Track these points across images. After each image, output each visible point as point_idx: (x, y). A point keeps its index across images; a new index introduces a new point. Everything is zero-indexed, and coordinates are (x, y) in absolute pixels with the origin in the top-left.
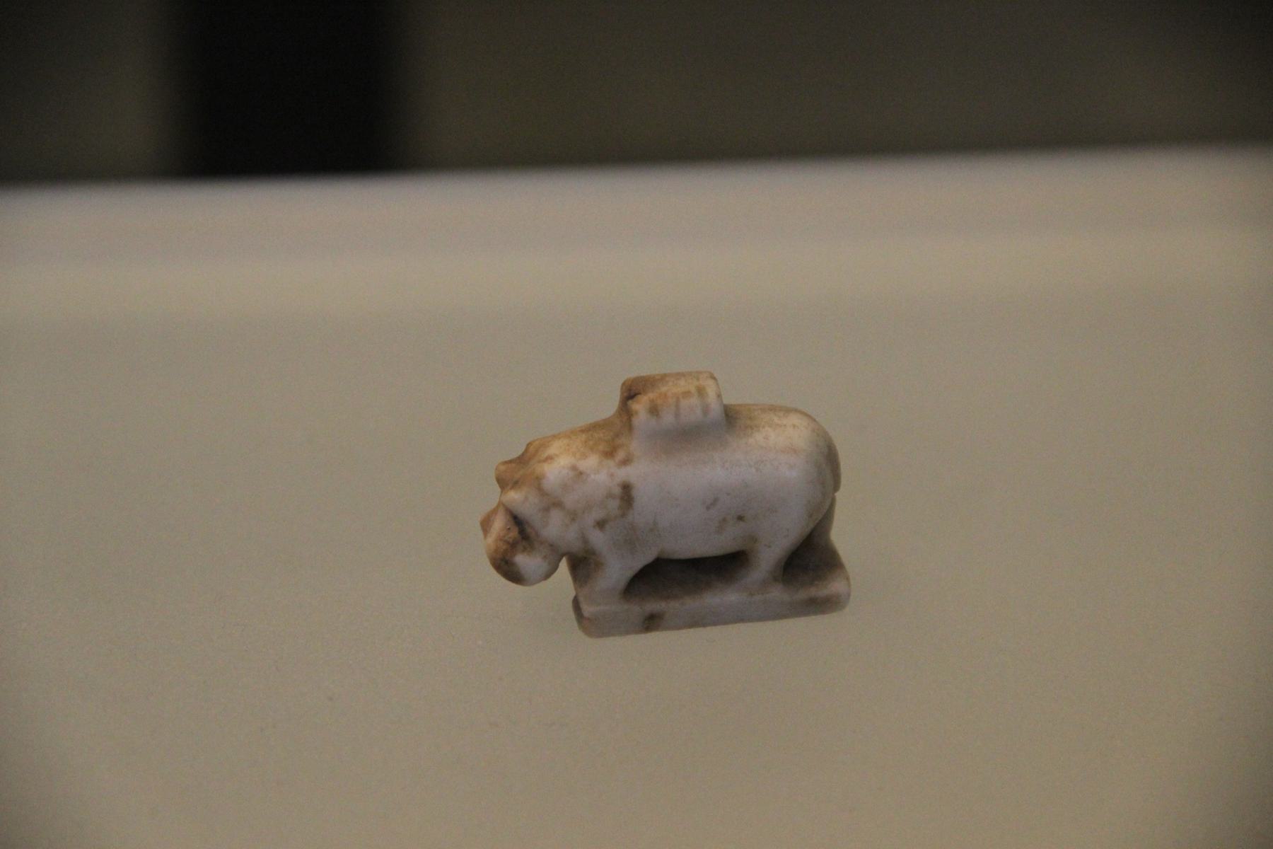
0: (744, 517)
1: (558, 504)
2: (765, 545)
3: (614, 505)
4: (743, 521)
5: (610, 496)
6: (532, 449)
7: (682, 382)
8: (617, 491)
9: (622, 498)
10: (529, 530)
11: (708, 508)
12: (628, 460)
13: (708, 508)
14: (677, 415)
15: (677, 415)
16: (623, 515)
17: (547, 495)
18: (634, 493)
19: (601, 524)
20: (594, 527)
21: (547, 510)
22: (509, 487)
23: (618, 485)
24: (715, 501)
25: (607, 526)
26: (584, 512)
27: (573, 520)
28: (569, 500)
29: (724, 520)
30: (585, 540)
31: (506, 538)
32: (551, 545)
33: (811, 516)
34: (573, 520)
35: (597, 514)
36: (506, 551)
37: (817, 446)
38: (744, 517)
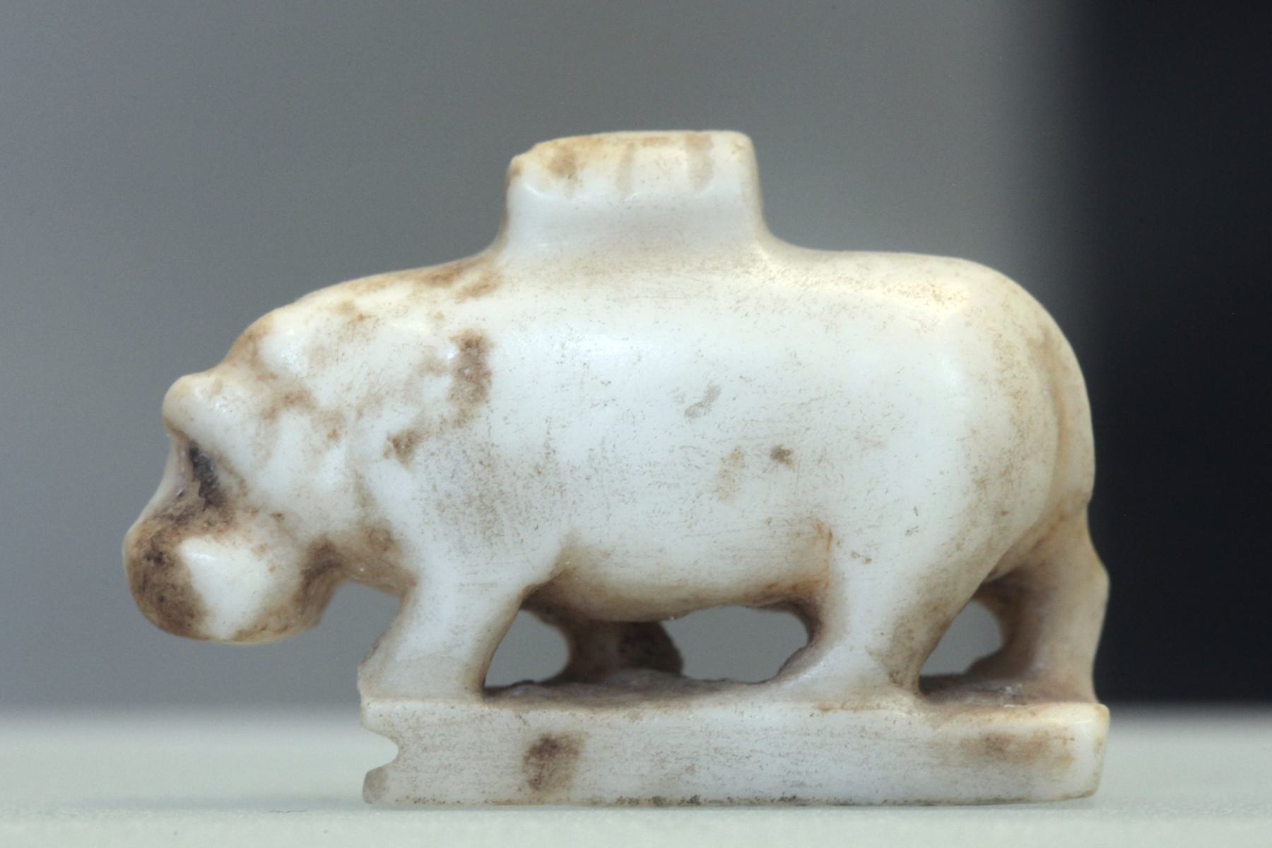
1: (296, 398)
2: (854, 555)
4: (788, 462)
5: (431, 367)
6: (202, 509)
9: (459, 373)
10: (224, 480)
11: (691, 414)
16: (462, 420)
17: (273, 377)
18: (495, 361)
19: (403, 446)
20: (386, 455)
21: (270, 415)
24: (712, 394)
25: (420, 454)
26: (360, 414)
30: (365, 498)
31: (170, 511)
32: (279, 516)
33: (982, 484)
34: (334, 436)
35: (395, 419)
38: (789, 453)
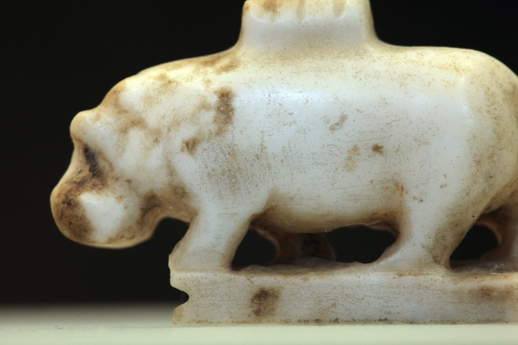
3: (208, 116)
4: (381, 152)
5: (204, 106)
7: (336, 63)
8: (214, 100)
10: (102, 163)
11: (333, 129)
12: (231, 66)
13: (333, 129)
14: (300, 12)
15: (300, 12)
16: (220, 132)
17: (126, 112)
18: (236, 103)
21: (124, 131)
23: (215, 93)
24: (343, 118)
25: (199, 149)
26: (169, 130)
27: (156, 141)
28: (233, 193)
29: (356, 149)
30: (172, 172)
31: (75, 179)
32: (129, 181)
34: (156, 141)
36: (70, 191)
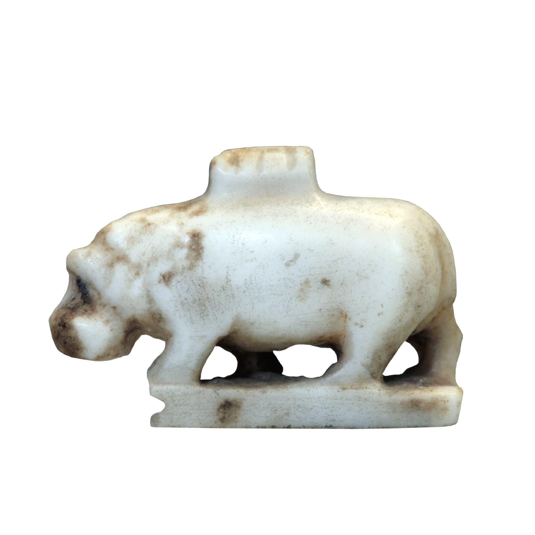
0: (329, 281)
1: (122, 258)
2: (356, 324)
4: (328, 285)
5: (178, 245)
9: (190, 247)
10: (91, 292)
11: (287, 265)
13: (287, 265)
16: (191, 267)
17: (112, 249)
18: (206, 242)
19: (167, 278)
21: (111, 265)
22: (137, 325)
24: (297, 256)
25: (174, 281)
26: (149, 265)
31: (69, 305)
32: (114, 308)
34: (137, 274)
35: (164, 267)
37: (357, 425)
38: (329, 281)
